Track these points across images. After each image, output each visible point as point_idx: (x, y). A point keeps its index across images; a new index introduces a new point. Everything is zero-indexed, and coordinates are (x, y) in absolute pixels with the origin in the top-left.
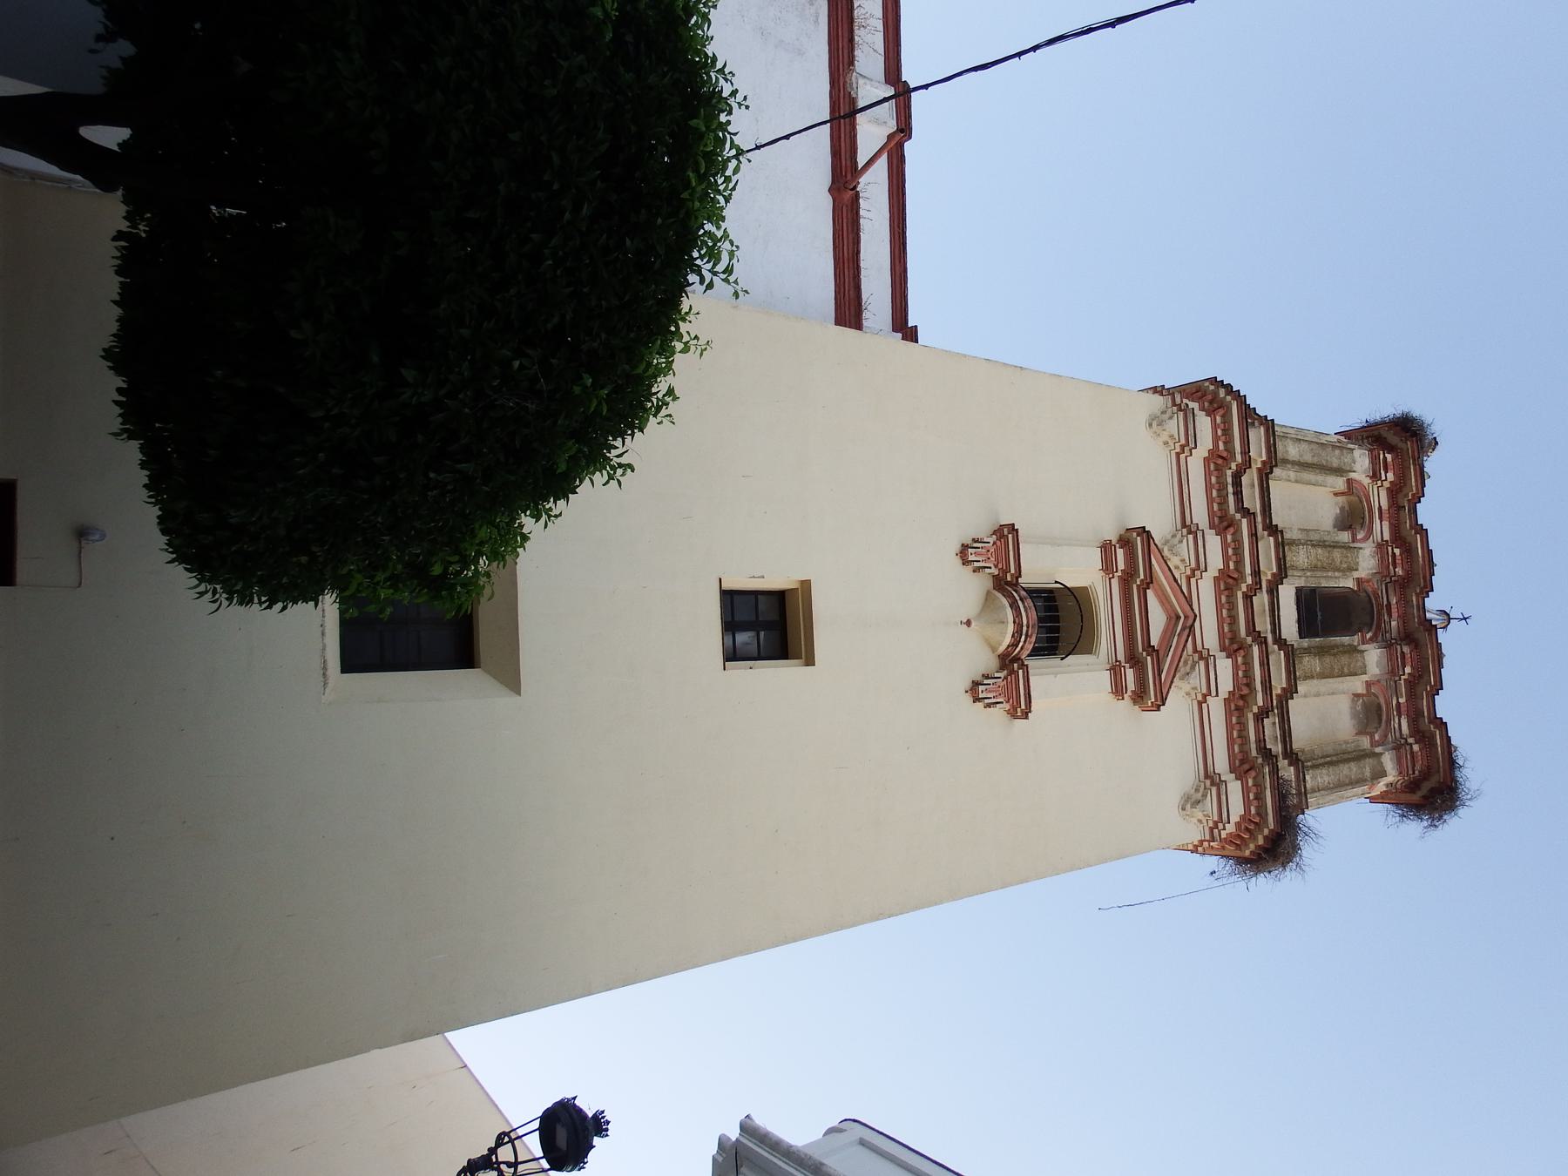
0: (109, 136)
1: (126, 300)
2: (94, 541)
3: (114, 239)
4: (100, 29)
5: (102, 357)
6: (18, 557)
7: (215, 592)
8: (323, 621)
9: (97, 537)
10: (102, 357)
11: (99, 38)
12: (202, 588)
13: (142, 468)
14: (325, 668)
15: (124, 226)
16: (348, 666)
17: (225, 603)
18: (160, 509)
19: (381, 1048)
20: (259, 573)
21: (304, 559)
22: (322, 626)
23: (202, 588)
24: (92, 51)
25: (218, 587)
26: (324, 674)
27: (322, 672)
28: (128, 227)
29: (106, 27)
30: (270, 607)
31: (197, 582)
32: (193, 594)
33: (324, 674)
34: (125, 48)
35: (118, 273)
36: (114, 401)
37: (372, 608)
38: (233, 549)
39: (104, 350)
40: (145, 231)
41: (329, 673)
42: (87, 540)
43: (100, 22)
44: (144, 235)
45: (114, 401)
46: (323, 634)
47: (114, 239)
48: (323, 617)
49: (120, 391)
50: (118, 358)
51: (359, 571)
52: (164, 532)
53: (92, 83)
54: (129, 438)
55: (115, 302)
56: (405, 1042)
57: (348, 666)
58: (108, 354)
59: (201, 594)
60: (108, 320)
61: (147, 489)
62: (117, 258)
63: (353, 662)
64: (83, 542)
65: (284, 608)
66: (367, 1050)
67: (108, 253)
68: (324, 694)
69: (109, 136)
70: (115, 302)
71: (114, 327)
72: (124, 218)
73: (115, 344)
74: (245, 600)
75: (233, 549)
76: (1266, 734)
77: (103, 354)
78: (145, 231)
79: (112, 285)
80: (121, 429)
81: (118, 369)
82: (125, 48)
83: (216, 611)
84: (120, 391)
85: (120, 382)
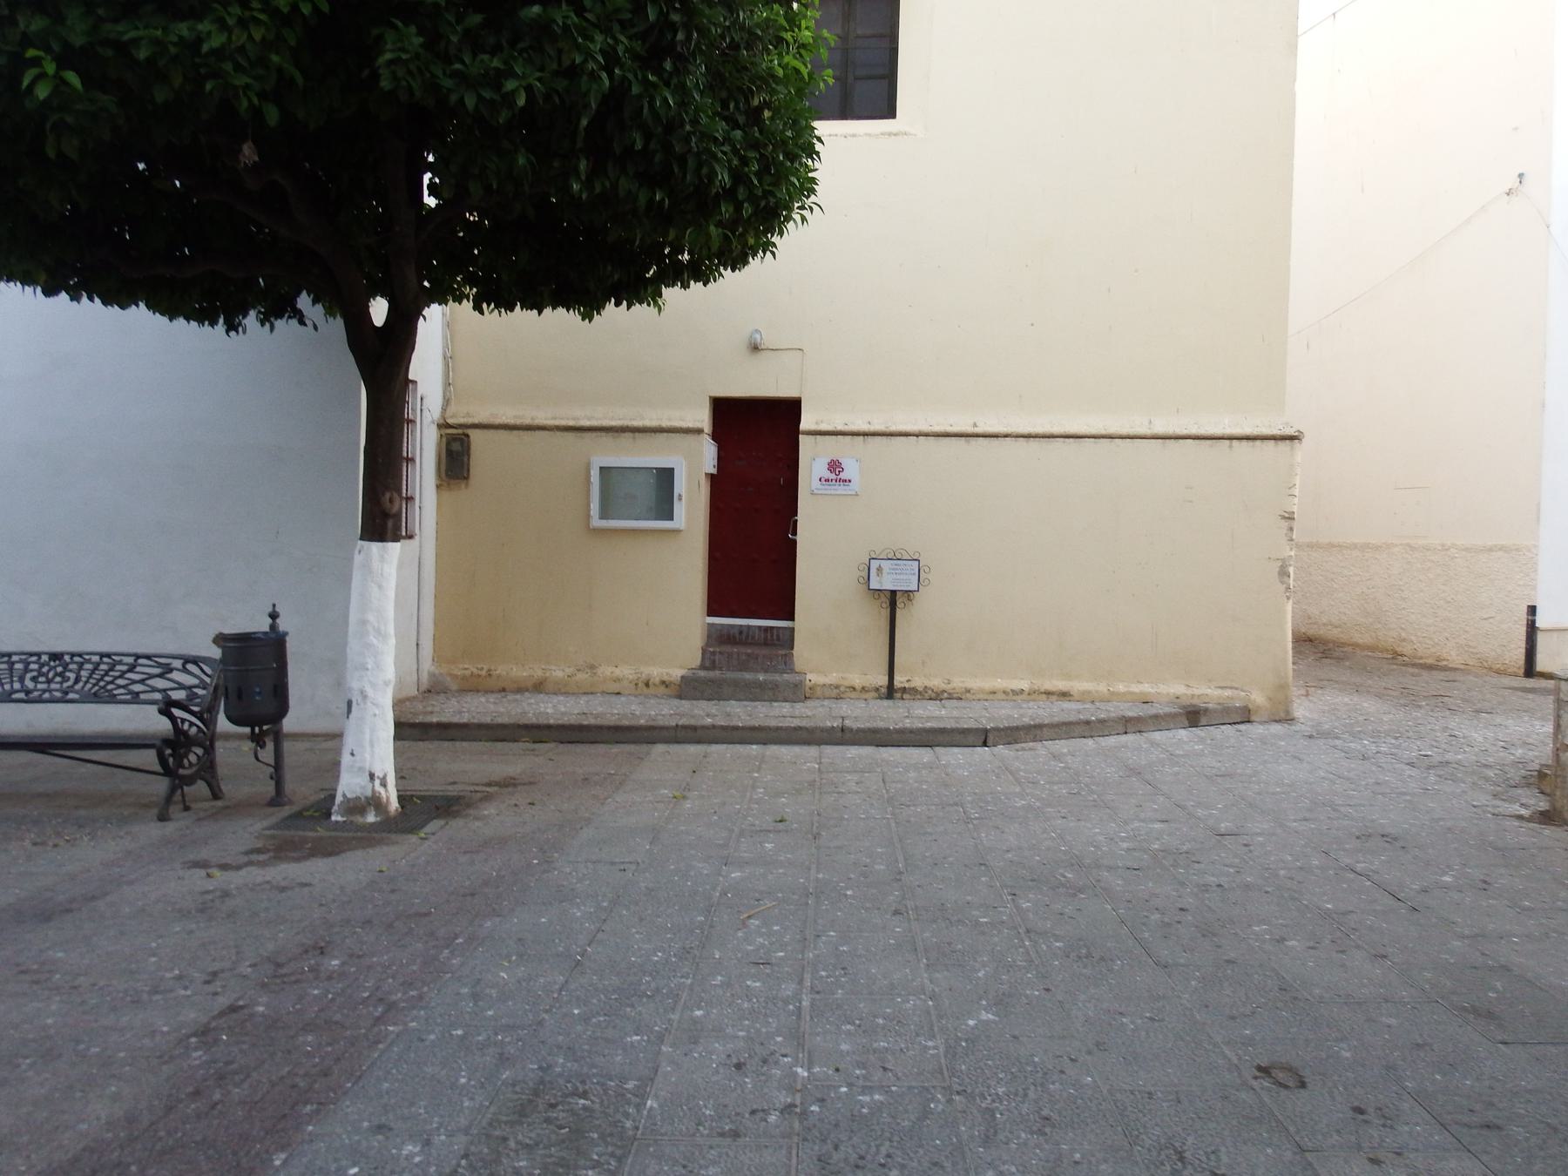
0: (379, 310)
1: (536, 304)
2: (761, 339)
3: (482, 313)
4: (294, 322)
5: (590, 322)
6: (777, 395)
7: (802, 208)
8: (841, 135)
9: (758, 336)
10: (590, 322)
11: (302, 322)
12: (797, 217)
13: (689, 287)
14: (890, 134)
15: (467, 305)
16: (890, 113)
17: (813, 198)
18: (725, 269)
19: (1295, 80)
20: (781, 158)
21: (767, 114)
22: (845, 137)
23: (797, 217)
24: (316, 328)
25: (796, 205)
26: (895, 135)
27: (893, 137)
28: (469, 301)
29: (290, 317)
30: (818, 154)
31: (792, 222)
32: (803, 229)
33: (895, 135)
34: (304, 301)
35: (512, 310)
36: (628, 309)
37: (824, 53)
38: (756, 182)
39: (583, 319)
40: (471, 289)
41: (894, 131)
42: (760, 344)
43: (287, 321)
44: (475, 290)
45: (628, 309)
46: (854, 136)
47: (482, 313)
48: (836, 135)
49: (617, 304)
50: (589, 305)
51: (780, 55)
52: (746, 263)
53: (336, 328)
54: (660, 296)
55: (540, 313)
56: (1296, 55)
57: (890, 113)
58: (587, 316)
59: (804, 219)
60: (560, 319)
61: (708, 283)
62: (500, 312)
63: (886, 108)
64: (763, 347)
65: (819, 139)
66: (1294, 95)
67: (495, 321)
68: (915, 135)
69: (379, 310)
70: (540, 313)
71: (561, 311)
72: (460, 304)
73: (576, 311)
74: (808, 187)
75: (756, 182)
76: (954, 757)
77: (587, 320)
78: (471, 289)
79: (521, 317)
80: (654, 307)
81: (599, 308)
82: (304, 301)
83: (819, 206)
84: (617, 304)
85: (610, 307)
